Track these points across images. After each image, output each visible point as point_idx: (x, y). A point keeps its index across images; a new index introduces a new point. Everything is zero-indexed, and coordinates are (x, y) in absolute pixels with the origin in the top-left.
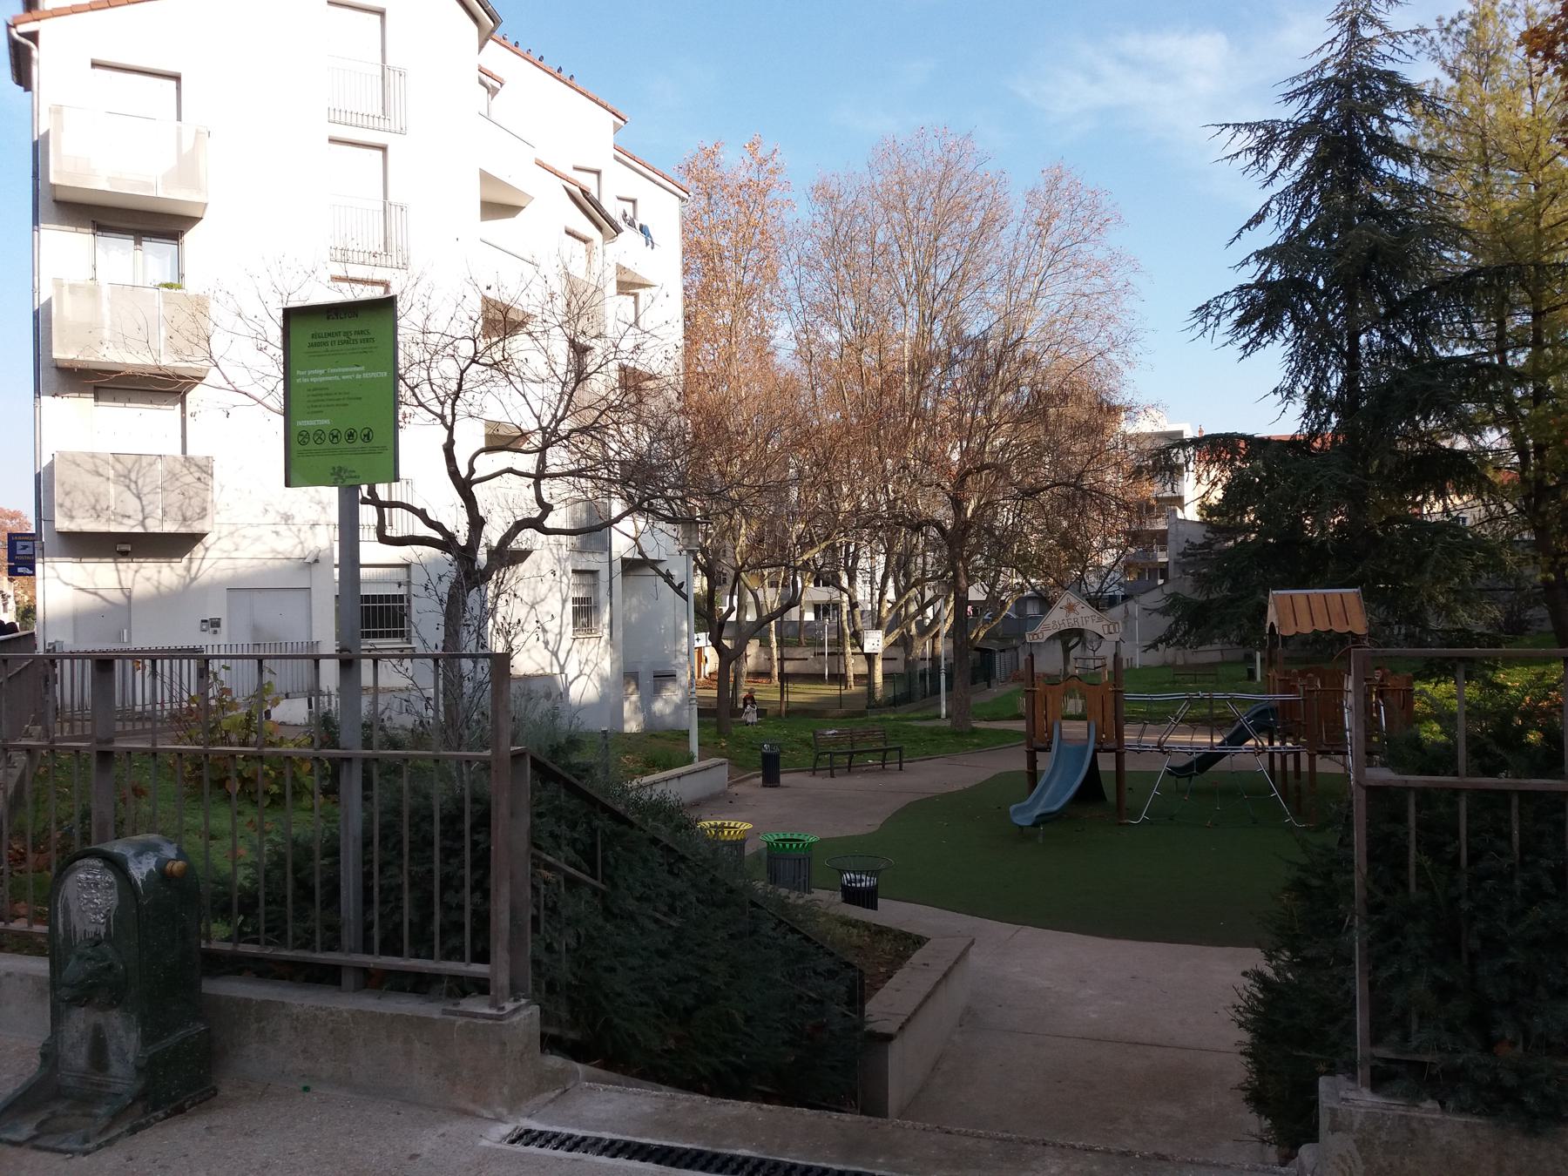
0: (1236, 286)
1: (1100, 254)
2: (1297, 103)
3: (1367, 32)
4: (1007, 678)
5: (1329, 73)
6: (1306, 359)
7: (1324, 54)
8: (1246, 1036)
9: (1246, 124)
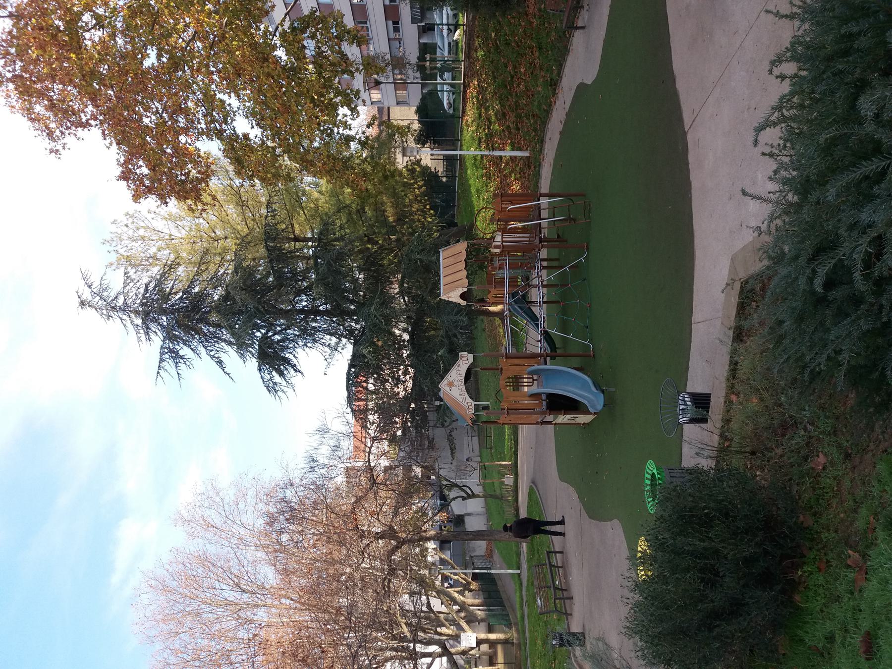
0: (257, 372)
1: (232, 492)
2: (152, 335)
3: (121, 301)
4: (490, 561)
5: (139, 321)
6: (308, 335)
7: (128, 324)
8: (637, 597)
9: (160, 362)
